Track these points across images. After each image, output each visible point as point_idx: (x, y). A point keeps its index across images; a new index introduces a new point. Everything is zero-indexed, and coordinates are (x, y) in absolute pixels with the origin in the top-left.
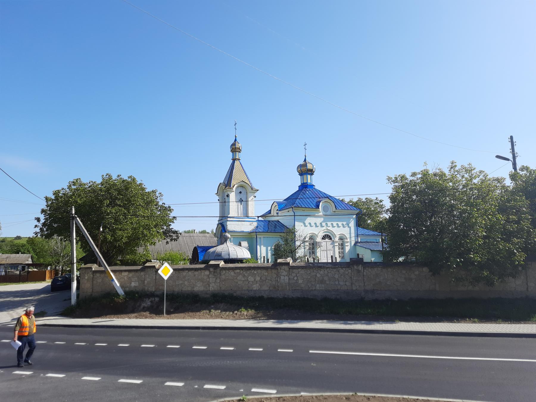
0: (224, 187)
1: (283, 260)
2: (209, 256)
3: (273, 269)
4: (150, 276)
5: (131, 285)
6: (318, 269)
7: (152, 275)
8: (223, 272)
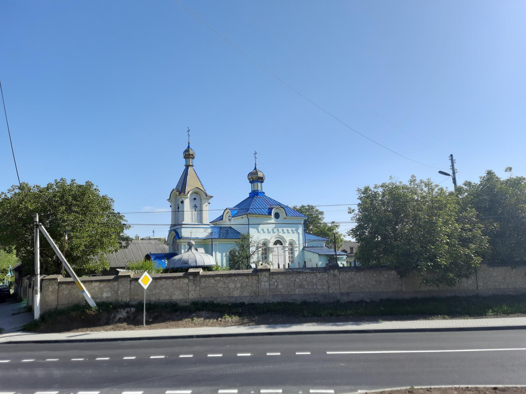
0: (178, 193)
1: (263, 267)
2: (174, 264)
3: (254, 275)
4: (124, 286)
5: (102, 296)
6: (297, 275)
7: (127, 285)
8: (203, 280)
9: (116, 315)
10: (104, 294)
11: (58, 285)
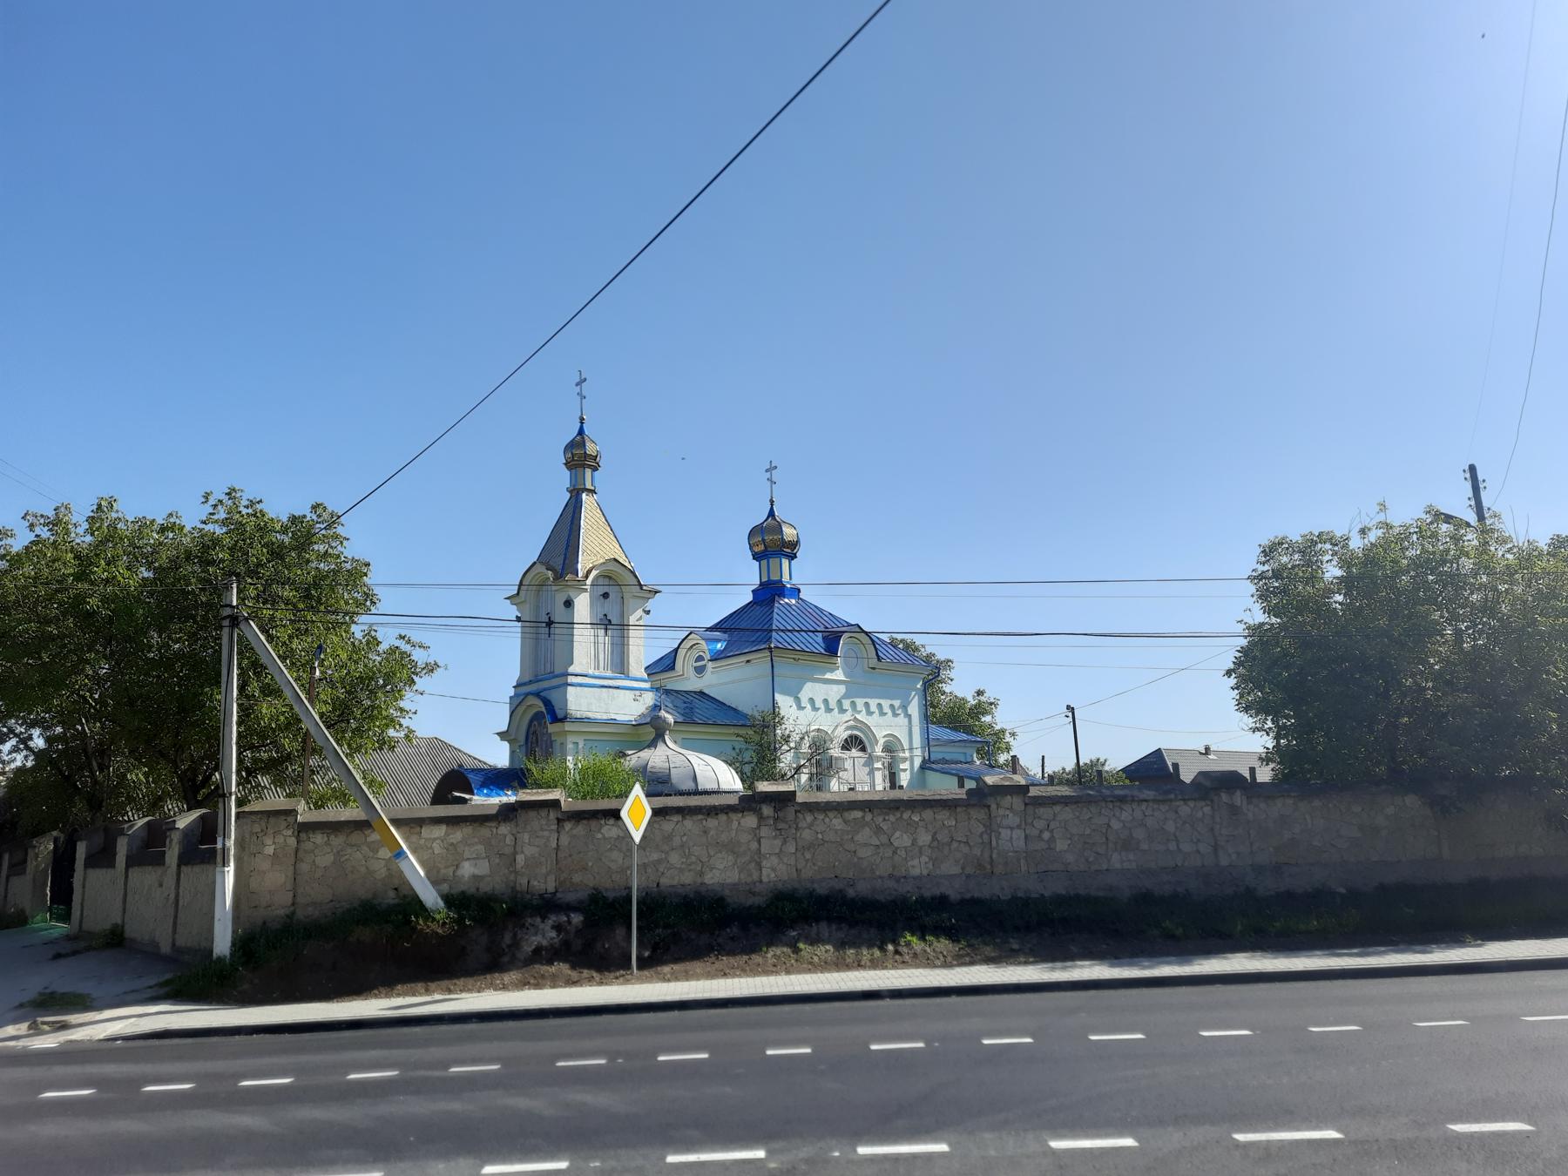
3: (974, 805)
4: (537, 837)
5: (459, 872)
6: (1114, 806)
7: (546, 833)
8: (805, 819)
9: (519, 936)
10: (463, 867)
11: (296, 833)
